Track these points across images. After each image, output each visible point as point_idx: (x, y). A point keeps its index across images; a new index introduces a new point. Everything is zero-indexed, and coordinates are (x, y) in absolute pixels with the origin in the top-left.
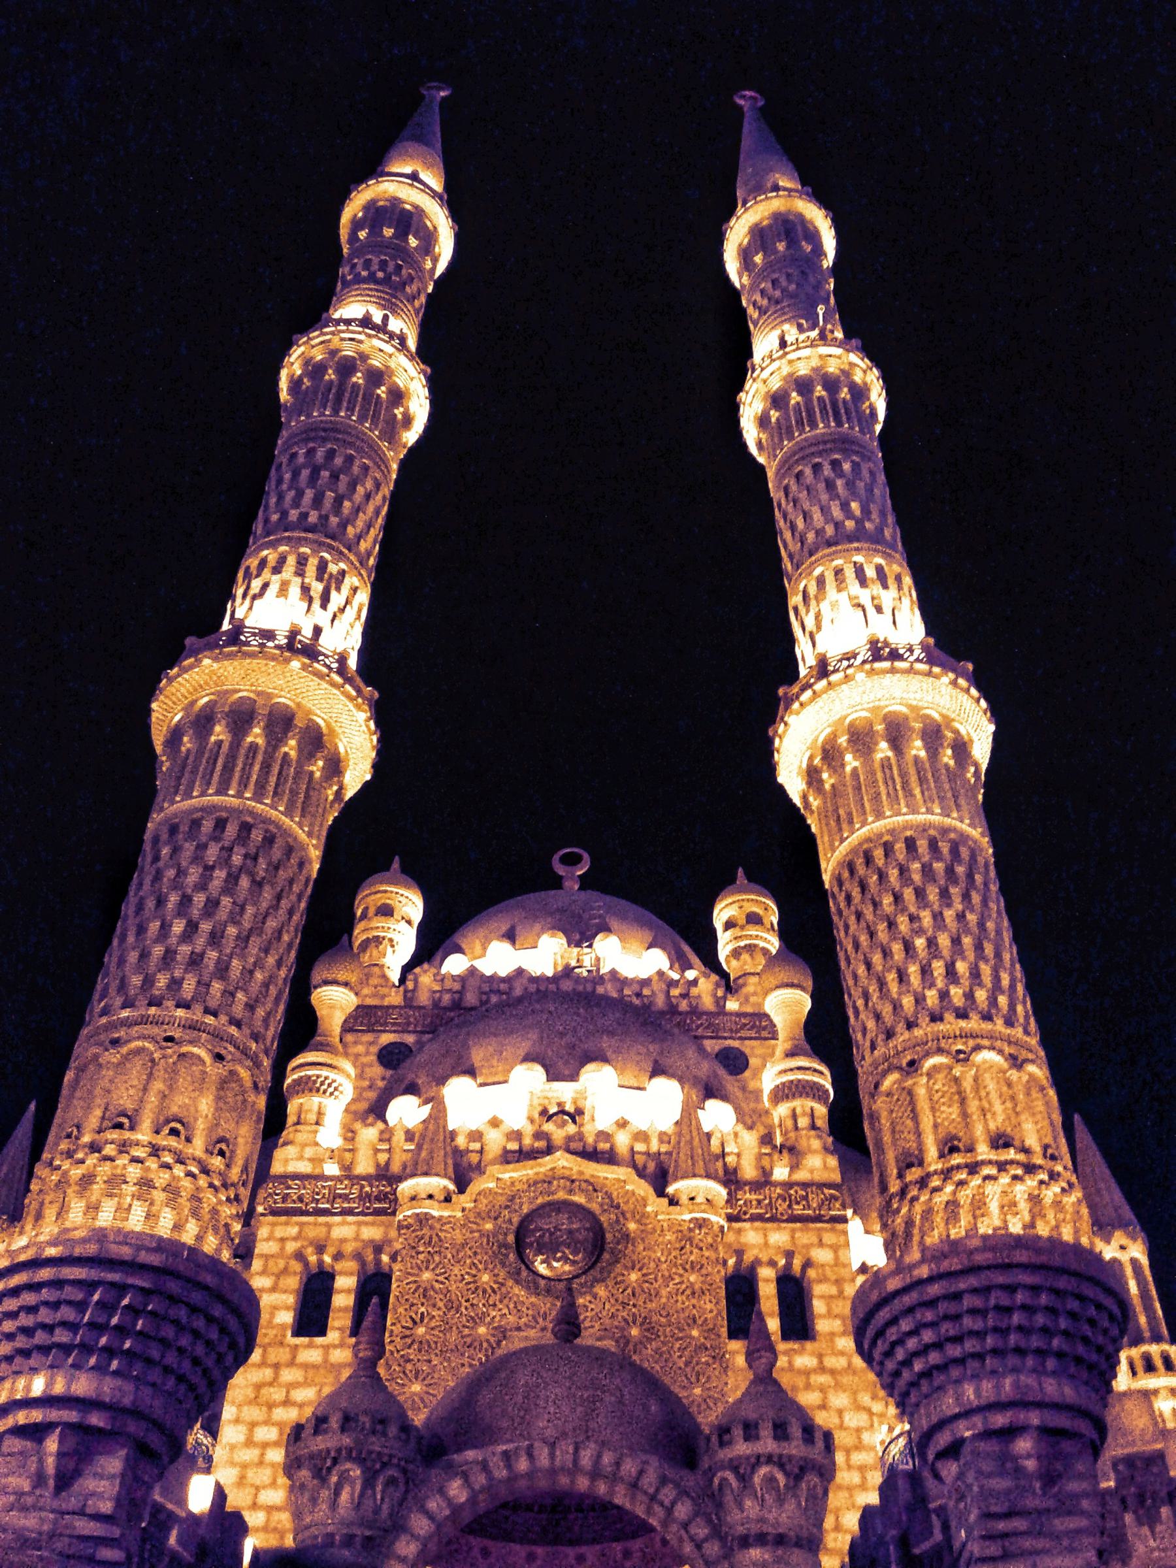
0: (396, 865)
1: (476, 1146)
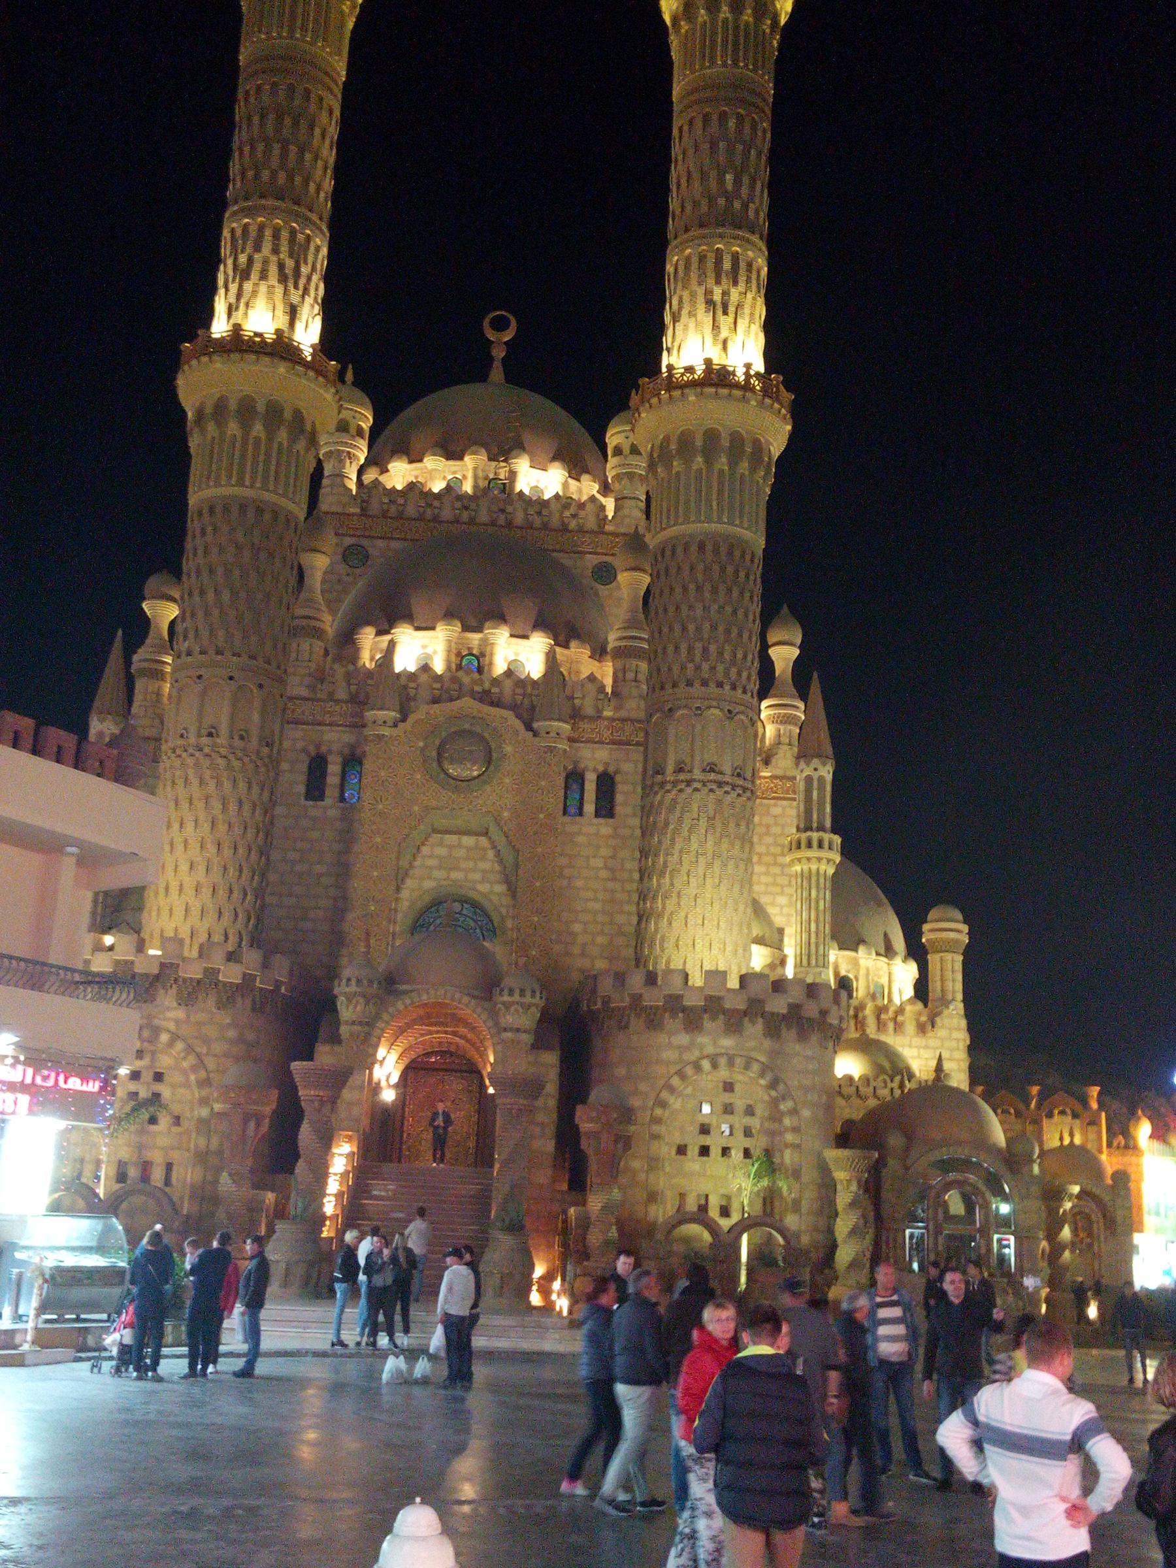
1: (412, 685)
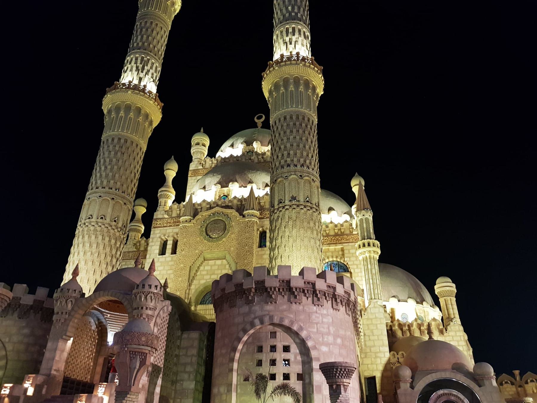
0: (202, 130)
